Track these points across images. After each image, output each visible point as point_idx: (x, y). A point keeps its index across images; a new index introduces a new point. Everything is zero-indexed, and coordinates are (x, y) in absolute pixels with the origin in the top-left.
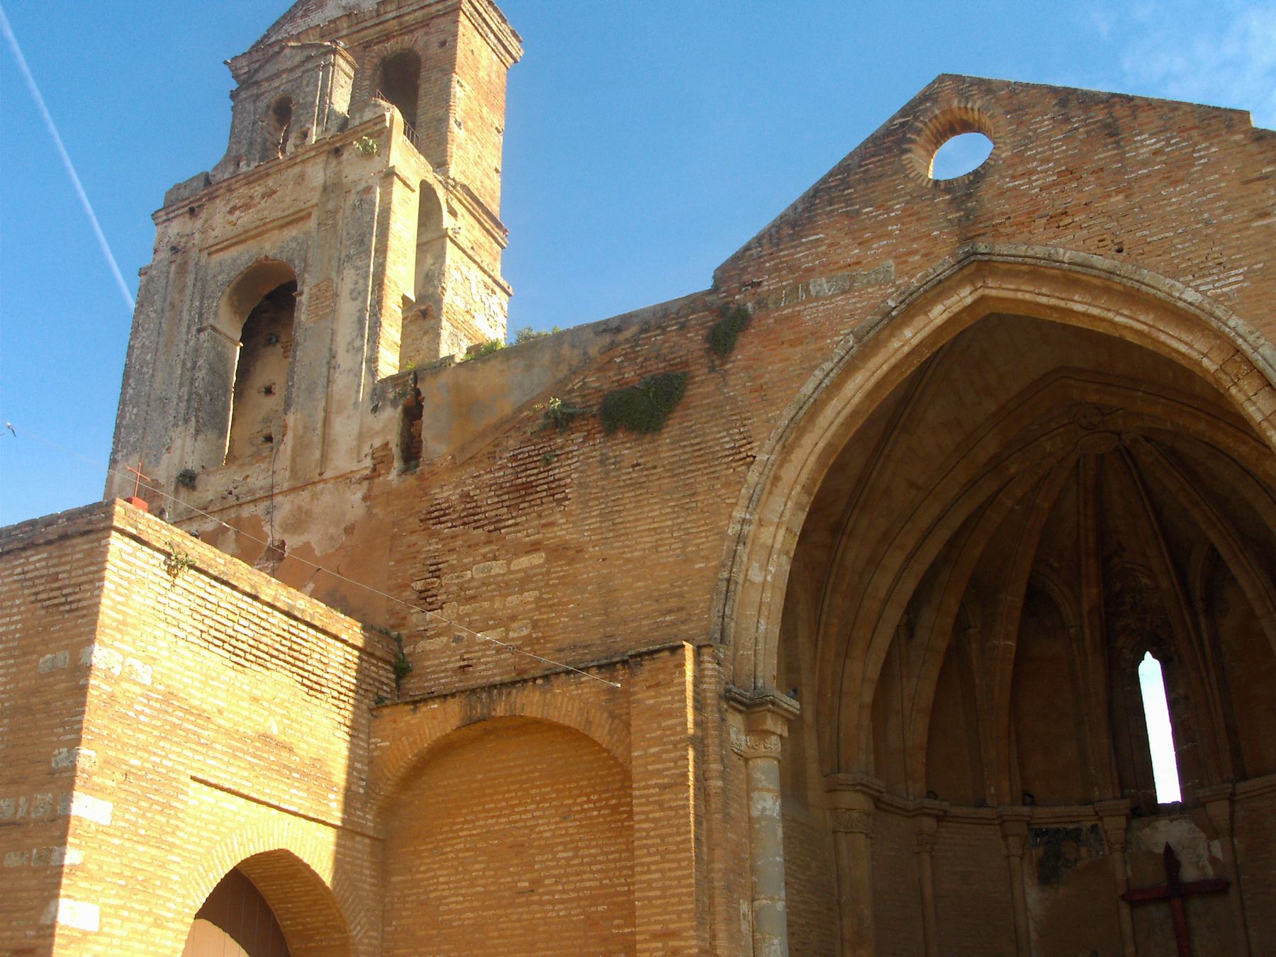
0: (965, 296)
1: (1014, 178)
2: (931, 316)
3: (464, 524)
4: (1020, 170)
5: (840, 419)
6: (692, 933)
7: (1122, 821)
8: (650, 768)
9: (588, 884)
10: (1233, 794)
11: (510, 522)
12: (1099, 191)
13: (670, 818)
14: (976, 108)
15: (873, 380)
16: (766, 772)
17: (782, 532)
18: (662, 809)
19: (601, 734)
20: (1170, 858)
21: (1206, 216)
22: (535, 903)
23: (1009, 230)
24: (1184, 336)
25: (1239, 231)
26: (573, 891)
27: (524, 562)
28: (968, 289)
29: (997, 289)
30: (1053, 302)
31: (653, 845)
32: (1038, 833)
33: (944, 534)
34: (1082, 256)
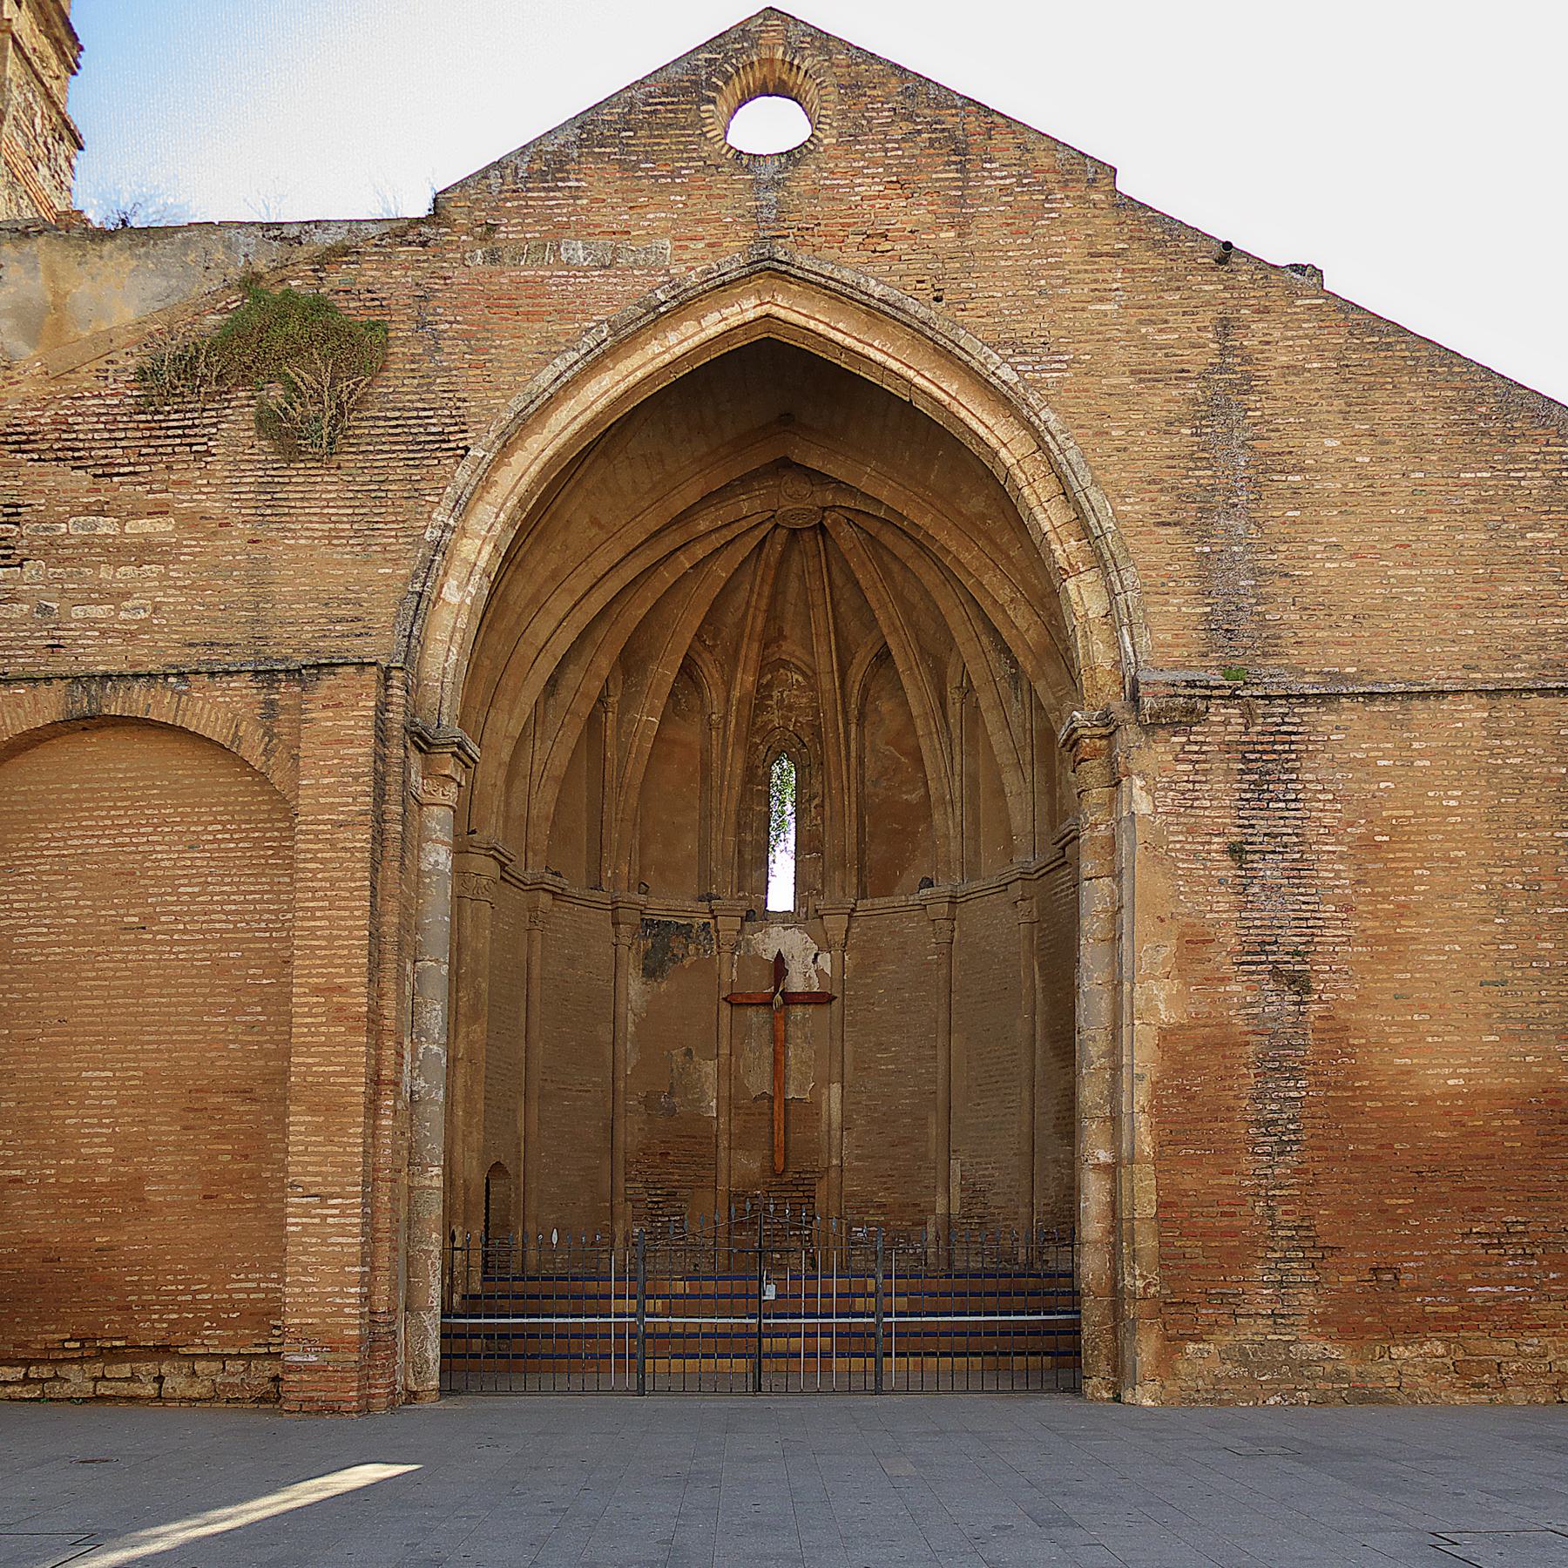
0: (745, 309)
3: (57, 459)
5: (576, 426)
6: (362, 989)
8: (322, 800)
9: (217, 926)
10: (853, 910)
11: (126, 470)
12: (929, 218)
13: (345, 860)
14: (804, 67)
15: (622, 387)
17: (488, 548)
18: (333, 848)
19: (253, 750)
20: (779, 966)
21: (1043, 282)
22: (148, 942)
23: (816, 241)
25: (1074, 310)
26: (197, 932)
27: (146, 525)
28: (754, 301)
30: (848, 342)
31: (321, 889)
32: (649, 924)
33: (613, 586)
34: (894, 295)
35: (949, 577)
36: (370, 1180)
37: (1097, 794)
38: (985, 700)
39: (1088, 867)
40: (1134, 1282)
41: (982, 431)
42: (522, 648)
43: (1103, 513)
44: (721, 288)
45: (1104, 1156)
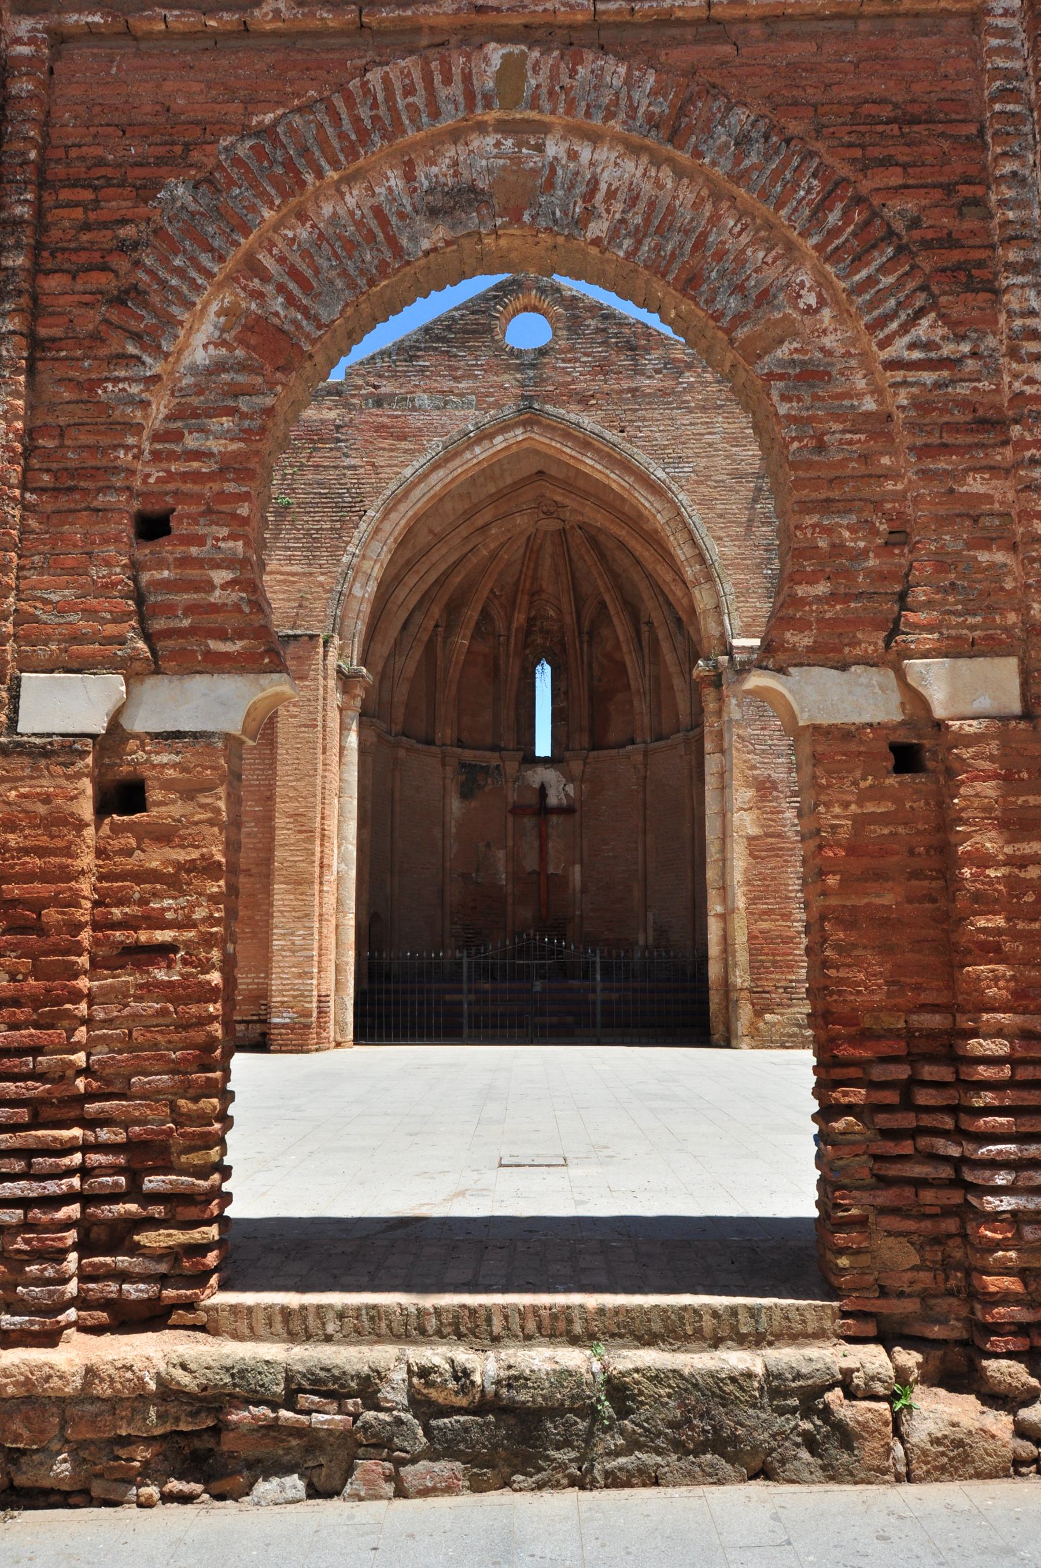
2: (495, 442)
5: (425, 499)
7: (516, 765)
17: (378, 566)
20: (542, 791)
24: (649, 496)
30: (573, 453)
33: (443, 567)
34: (598, 429)
38: (662, 634)
39: (708, 746)
41: (647, 505)
42: (389, 605)
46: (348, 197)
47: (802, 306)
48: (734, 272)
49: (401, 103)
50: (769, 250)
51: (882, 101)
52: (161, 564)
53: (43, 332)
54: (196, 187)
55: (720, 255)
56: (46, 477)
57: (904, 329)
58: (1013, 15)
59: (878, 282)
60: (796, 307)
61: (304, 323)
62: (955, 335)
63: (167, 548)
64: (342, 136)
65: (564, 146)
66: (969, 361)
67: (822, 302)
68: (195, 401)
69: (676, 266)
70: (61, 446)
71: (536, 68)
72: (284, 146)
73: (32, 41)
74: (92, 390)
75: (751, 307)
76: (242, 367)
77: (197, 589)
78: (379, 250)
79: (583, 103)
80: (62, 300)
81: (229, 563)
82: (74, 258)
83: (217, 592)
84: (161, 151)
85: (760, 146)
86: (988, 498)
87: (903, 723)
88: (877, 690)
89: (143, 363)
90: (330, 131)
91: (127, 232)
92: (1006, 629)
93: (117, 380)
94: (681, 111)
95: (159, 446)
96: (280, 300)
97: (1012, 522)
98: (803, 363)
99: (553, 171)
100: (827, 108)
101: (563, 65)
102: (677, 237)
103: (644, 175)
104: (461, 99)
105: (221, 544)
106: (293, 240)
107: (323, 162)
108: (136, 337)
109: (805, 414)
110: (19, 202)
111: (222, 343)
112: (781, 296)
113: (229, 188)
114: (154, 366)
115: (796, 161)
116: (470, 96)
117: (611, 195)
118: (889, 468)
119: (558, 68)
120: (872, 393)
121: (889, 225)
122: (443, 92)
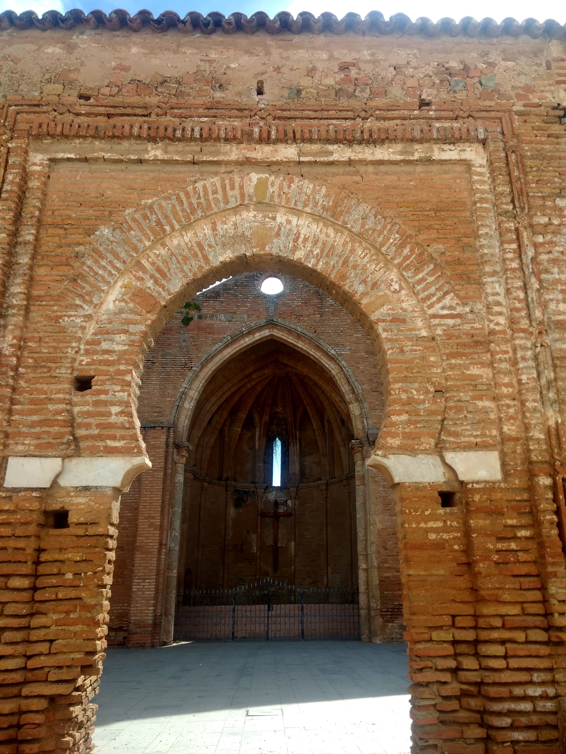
0: (266, 333)
1: (288, 300)
4: (291, 298)
16: (181, 468)
17: (197, 393)
28: (268, 330)
29: (278, 333)
33: (229, 393)
35: (323, 392)
36: (158, 574)
37: (359, 463)
38: (334, 426)
39: (357, 483)
40: (373, 605)
43: (359, 389)
44: (260, 328)
45: (364, 566)
46: (185, 237)
47: (392, 289)
48: (361, 274)
49: (211, 197)
50: (377, 265)
51: (426, 202)
52: (86, 403)
53: (35, 293)
54: (114, 230)
55: (355, 267)
56: (31, 361)
57: (439, 300)
58: (484, 167)
59: (426, 280)
60: (390, 290)
61: (162, 292)
62: (462, 303)
63: (89, 396)
64: (183, 210)
65: (285, 218)
66: (469, 315)
67: (401, 288)
68: (108, 326)
69: (335, 271)
70: (40, 346)
71: (273, 184)
72: (156, 214)
73: (41, 164)
74: (57, 321)
75: (369, 289)
76: (132, 311)
77: (103, 415)
78: (199, 261)
79: (294, 200)
80: (45, 279)
81: (120, 403)
82: (53, 259)
83: (113, 417)
84: (98, 213)
85: (372, 219)
86: (481, 377)
87: (445, 482)
88: (431, 466)
89: (84, 309)
90: (178, 208)
91: (81, 249)
92: (491, 437)
93: (69, 316)
94: (336, 205)
95: (89, 347)
96: (152, 281)
97: (492, 387)
98: (393, 314)
99: (280, 229)
100: (402, 204)
101: (285, 183)
102: (336, 259)
103: (321, 231)
104: (238, 196)
105: (116, 394)
106: (159, 255)
107: (174, 222)
108: (81, 296)
109: (394, 337)
110: (29, 234)
111: (123, 300)
112: (383, 285)
113: (129, 231)
114: (89, 310)
115: (389, 227)
116: (242, 195)
117: (306, 240)
118: (434, 362)
119: (283, 184)
120: (425, 328)
121: (431, 255)
122: (230, 193)
